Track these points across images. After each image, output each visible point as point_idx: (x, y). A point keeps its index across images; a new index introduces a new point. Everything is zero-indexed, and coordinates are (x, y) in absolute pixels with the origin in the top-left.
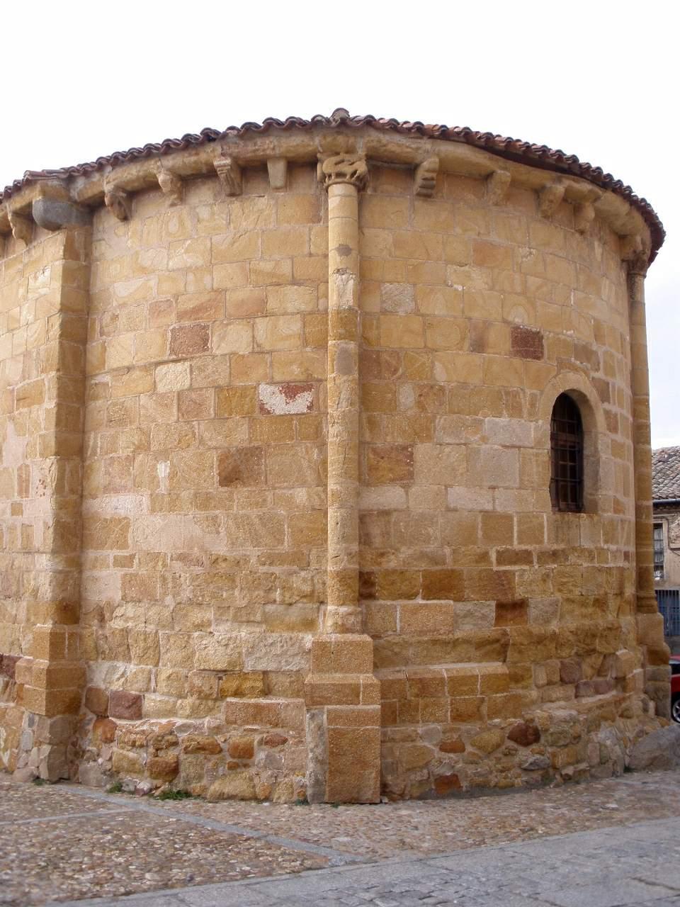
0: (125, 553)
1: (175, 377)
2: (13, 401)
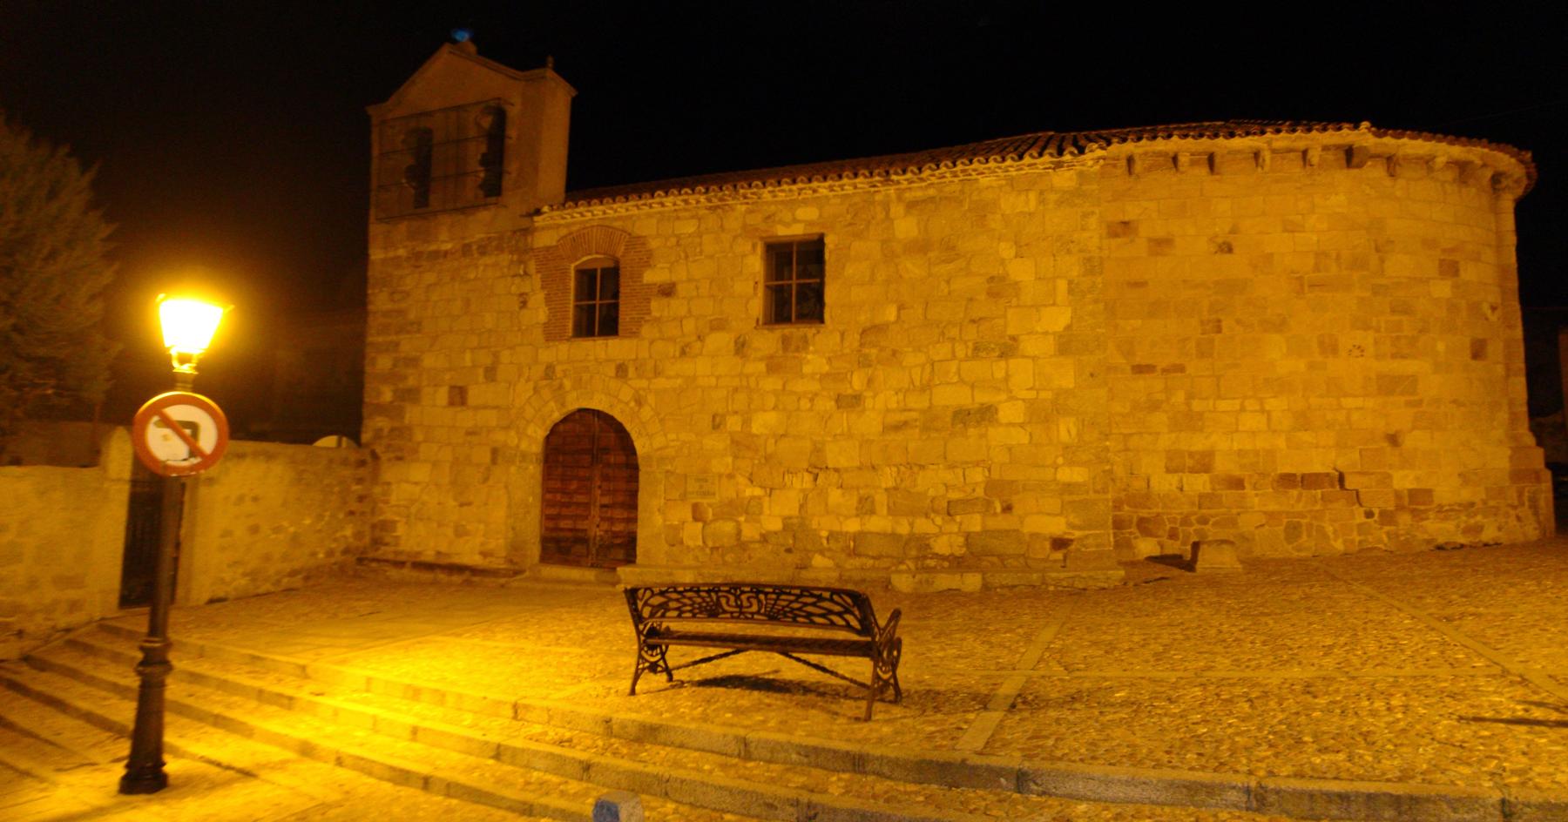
0: (1416, 398)
1: (1443, 289)
2: (1302, 285)
